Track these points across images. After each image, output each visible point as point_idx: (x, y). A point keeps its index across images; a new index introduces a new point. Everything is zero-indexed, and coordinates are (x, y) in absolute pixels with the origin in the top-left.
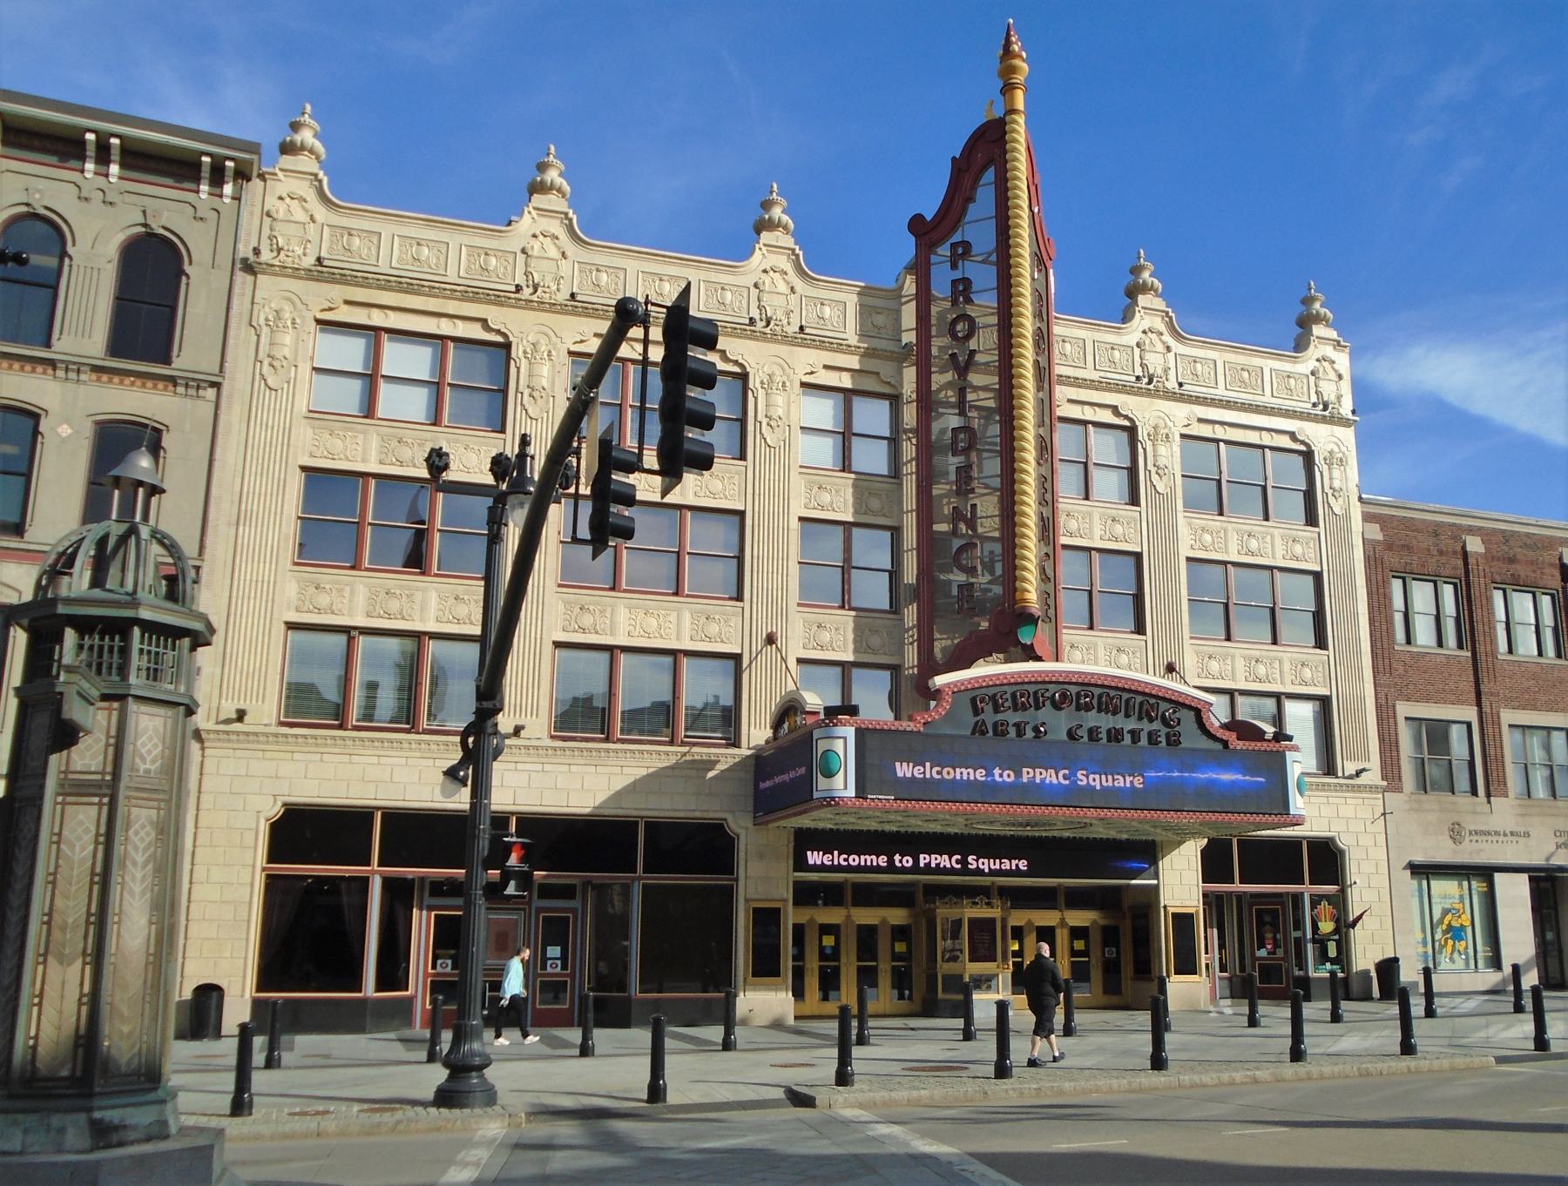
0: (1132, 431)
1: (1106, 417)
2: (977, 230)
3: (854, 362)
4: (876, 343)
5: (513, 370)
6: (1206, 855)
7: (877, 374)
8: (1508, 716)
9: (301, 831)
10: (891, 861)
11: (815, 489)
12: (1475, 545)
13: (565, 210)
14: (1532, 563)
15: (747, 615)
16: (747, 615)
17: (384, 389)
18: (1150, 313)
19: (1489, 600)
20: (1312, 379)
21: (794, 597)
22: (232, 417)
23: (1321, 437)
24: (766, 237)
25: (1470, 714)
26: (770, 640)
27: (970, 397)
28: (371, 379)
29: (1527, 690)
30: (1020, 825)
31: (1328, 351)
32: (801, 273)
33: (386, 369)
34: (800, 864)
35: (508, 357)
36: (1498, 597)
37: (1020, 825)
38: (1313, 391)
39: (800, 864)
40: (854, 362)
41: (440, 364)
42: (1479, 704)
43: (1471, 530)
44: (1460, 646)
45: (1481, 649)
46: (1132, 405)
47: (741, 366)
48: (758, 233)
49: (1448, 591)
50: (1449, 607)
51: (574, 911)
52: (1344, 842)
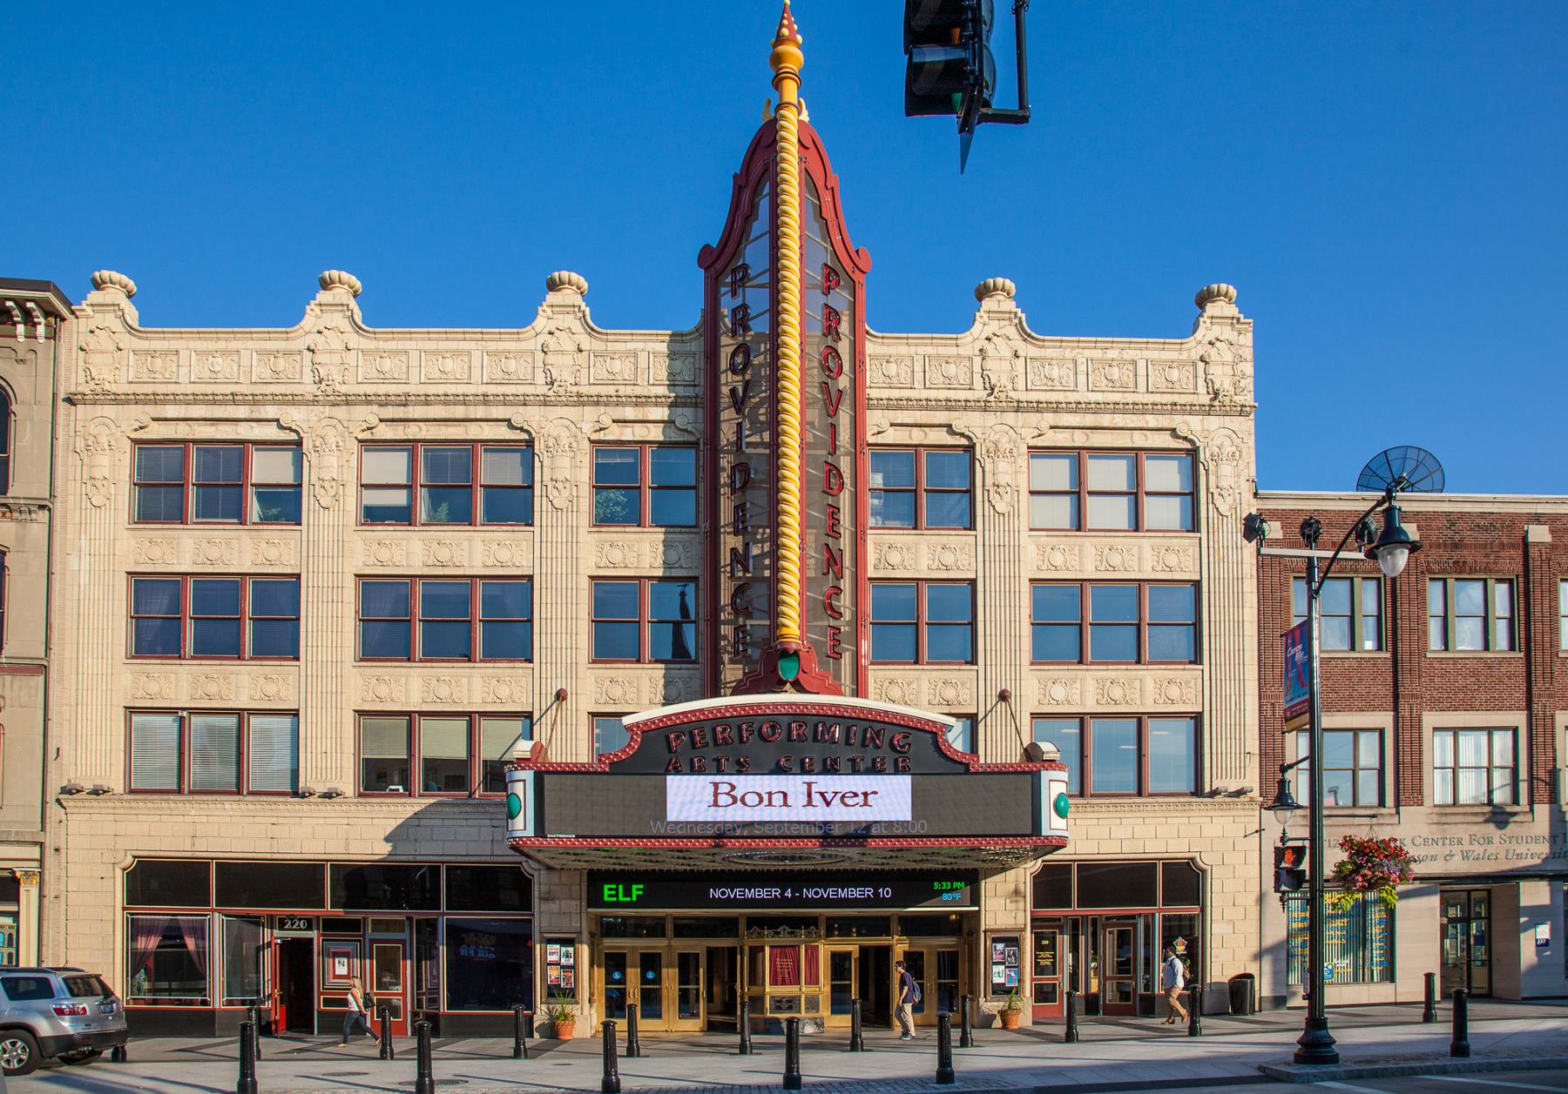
0: (1193, 453)
1: (1165, 440)
2: (754, 255)
3: (662, 413)
4: (681, 391)
5: (978, 470)
6: (1038, 880)
7: (949, 426)
8: (1430, 719)
9: (1185, 880)
10: (876, 894)
11: (607, 546)
12: (1539, 534)
13: (1237, 314)
14: (1485, 546)
15: (537, 675)
16: (537, 675)
17: (1091, 503)
18: (998, 316)
19: (1421, 594)
20: (1201, 365)
21: (1026, 656)
22: (67, 533)
23: (1211, 433)
24: (987, 304)
25: (1385, 719)
26: (1003, 696)
27: (766, 436)
28: (1077, 494)
29: (1463, 689)
30: (776, 858)
31: (1227, 333)
32: (1026, 337)
33: (1149, 485)
34: (595, 899)
35: (973, 459)
36: (1434, 591)
37: (776, 858)
38: (1201, 381)
39: (595, 899)
40: (662, 413)
41: (1136, 474)
42: (1396, 709)
43: (1538, 519)
44: (1512, 648)
45: (1403, 648)
46: (1192, 425)
47: (968, 438)
48: (980, 299)
49: (1501, 592)
50: (1501, 605)
51: (403, 942)
52: (1206, 860)
